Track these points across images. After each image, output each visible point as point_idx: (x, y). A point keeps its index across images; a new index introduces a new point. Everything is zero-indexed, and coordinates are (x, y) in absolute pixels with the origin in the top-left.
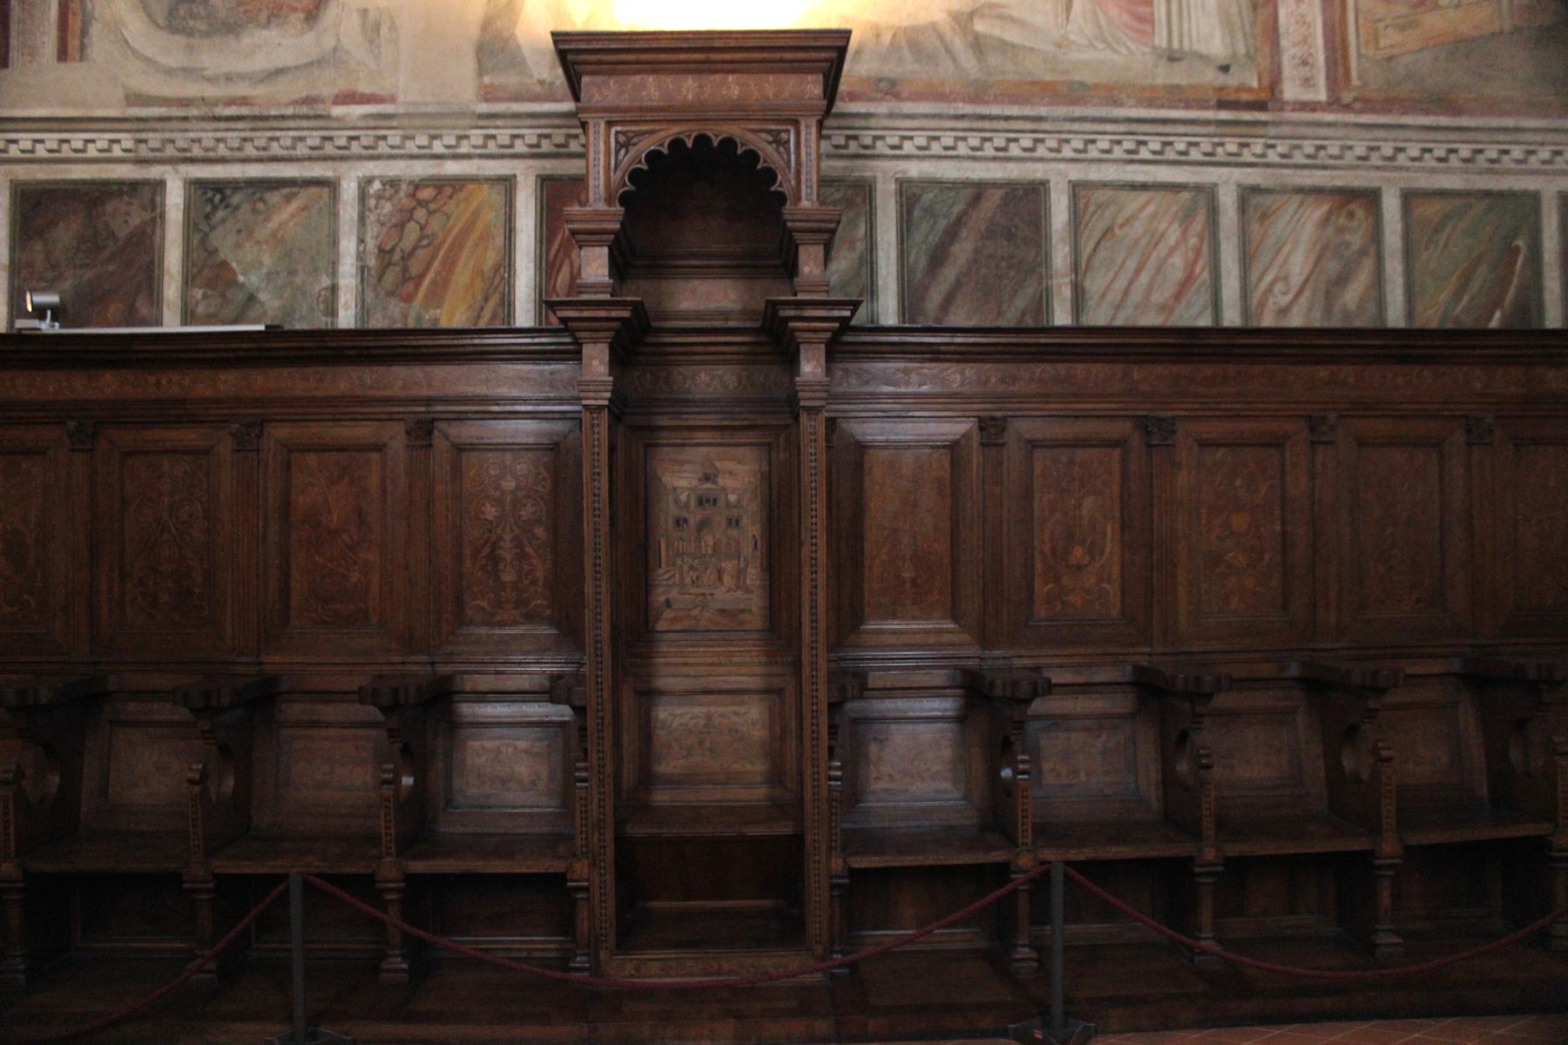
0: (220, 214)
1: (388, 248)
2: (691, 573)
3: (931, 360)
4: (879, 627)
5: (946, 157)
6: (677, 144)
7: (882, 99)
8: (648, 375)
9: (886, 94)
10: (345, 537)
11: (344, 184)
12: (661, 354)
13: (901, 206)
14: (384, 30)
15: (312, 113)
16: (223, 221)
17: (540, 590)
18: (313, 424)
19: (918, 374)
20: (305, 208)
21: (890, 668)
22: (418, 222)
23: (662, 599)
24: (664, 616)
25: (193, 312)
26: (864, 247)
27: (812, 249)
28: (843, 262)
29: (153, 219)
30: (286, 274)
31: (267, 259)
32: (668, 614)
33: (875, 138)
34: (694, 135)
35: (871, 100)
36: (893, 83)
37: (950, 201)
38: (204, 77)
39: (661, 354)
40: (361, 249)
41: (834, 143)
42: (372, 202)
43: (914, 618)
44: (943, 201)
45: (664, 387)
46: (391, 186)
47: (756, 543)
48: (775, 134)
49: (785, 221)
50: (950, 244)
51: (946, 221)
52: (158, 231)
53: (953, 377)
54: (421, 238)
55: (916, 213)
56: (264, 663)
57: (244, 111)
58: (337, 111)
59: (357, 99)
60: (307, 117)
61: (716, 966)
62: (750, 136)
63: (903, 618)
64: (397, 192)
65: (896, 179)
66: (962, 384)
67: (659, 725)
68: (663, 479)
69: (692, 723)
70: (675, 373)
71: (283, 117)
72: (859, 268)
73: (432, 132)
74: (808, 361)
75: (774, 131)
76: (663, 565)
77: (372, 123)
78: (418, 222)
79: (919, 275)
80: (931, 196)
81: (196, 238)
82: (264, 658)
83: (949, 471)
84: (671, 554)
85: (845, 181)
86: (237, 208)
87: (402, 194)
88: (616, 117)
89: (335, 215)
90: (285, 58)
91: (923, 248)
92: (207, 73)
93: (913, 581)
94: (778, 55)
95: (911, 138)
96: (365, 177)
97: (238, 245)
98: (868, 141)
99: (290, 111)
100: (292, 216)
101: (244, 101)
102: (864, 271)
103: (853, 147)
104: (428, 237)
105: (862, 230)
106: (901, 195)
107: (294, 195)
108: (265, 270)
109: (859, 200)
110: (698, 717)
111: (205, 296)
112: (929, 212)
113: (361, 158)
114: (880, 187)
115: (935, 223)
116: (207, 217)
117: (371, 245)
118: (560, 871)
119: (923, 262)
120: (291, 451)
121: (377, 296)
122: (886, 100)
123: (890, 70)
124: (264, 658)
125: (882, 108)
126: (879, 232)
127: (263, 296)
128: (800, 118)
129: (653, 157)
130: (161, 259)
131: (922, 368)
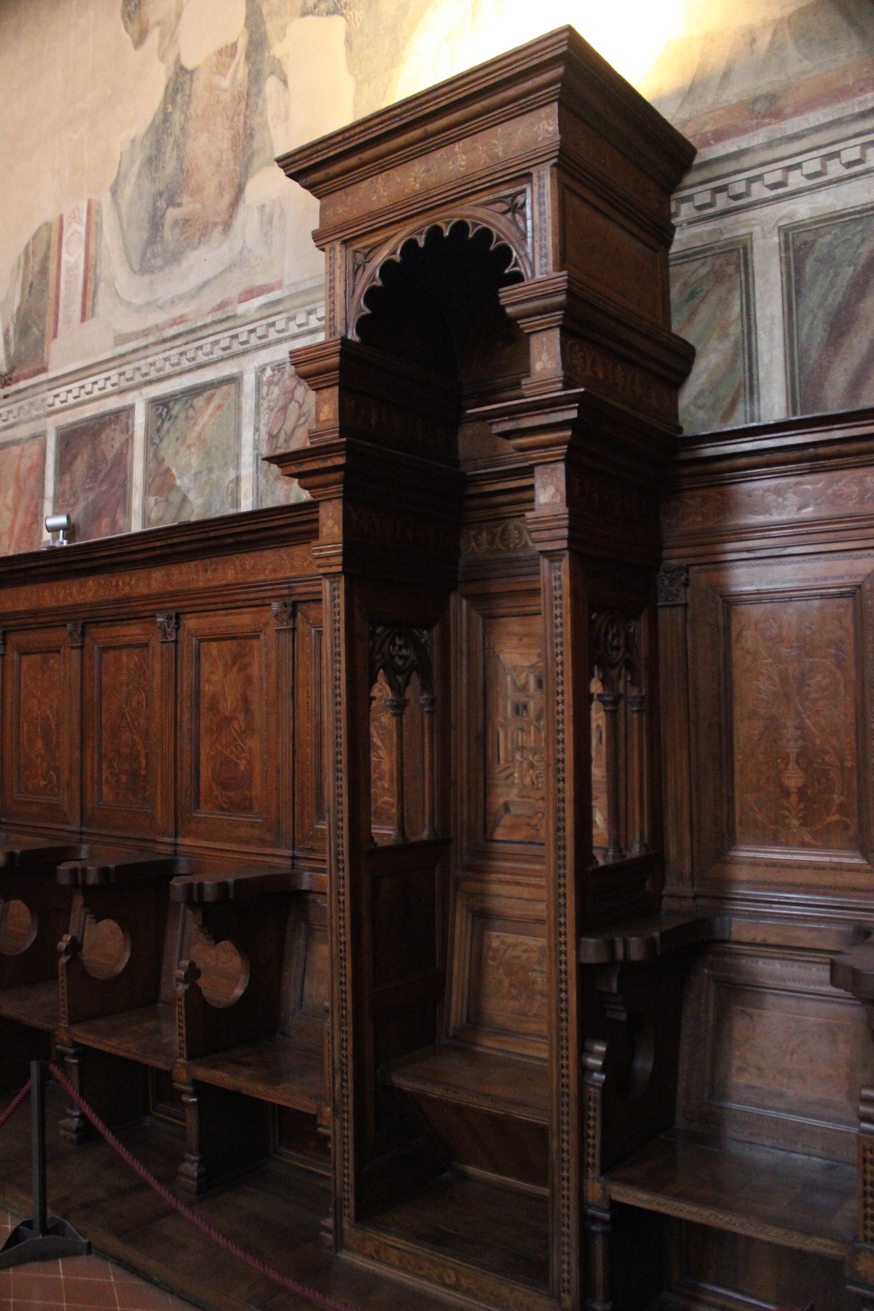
0: (167, 425)
1: (275, 433)
2: (531, 771)
3: (813, 471)
4: (752, 854)
5: (850, 177)
6: (410, 246)
7: (759, 126)
8: (485, 534)
9: (764, 117)
10: (236, 726)
11: (245, 377)
12: (489, 507)
13: (788, 264)
14: (276, 219)
15: (224, 316)
16: (168, 431)
17: (386, 785)
18: (211, 613)
19: (795, 493)
20: (219, 407)
21: (764, 916)
22: (297, 402)
23: (501, 800)
24: (503, 822)
25: (149, 519)
26: (739, 329)
27: (543, 337)
28: (712, 356)
29: (127, 440)
30: (206, 472)
31: (194, 461)
32: (506, 820)
33: (750, 181)
34: (426, 228)
35: (745, 131)
36: (772, 97)
37: (857, 239)
38: (158, 306)
39: (489, 507)
40: (257, 438)
41: (697, 203)
42: (265, 390)
43: (803, 845)
44: (845, 241)
45: (500, 546)
46: (279, 370)
47: (601, 734)
48: (510, 199)
49: (503, 307)
50: (859, 300)
51: (852, 268)
52: (130, 451)
53: (846, 490)
54: (299, 418)
55: (809, 268)
56: (180, 845)
57: (180, 328)
58: (241, 309)
59: (255, 293)
60: (221, 321)
61: (454, 1278)
62: (481, 213)
63: (787, 844)
64: (283, 374)
65: (780, 228)
66: (861, 499)
67: (491, 954)
68: (501, 657)
69: (525, 956)
70: (511, 527)
71: (205, 326)
72: (734, 361)
73: (309, 308)
74: (544, 487)
75: (506, 197)
76: (502, 762)
77: (265, 313)
78: (297, 402)
79: (814, 354)
80: (828, 238)
81: (153, 449)
82: (179, 841)
83: (851, 631)
84: (509, 746)
85: (711, 249)
86: (176, 417)
87: (286, 376)
88: (349, 233)
89: (238, 408)
90: (208, 272)
91: (820, 313)
92: (160, 303)
93: (801, 792)
94: (496, 98)
95: (799, 166)
96: (260, 367)
97: (177, 453)
98: (740, 188)
99: (209, 320)
100: (211, 416)
101: (181, 320)
102: (739, 365)
103: (722, 202)
104: (304, 414)
105: (736, 308)
106: (787, 249)
107: (212, 396)
108: (193, 472)
109: (731, 269)
110: (533, 951)
111: (156, 503)
112: (828, 261)
113: (257, 348)
114: (758, 245)
115: (837, 275)
116: (158, 430)
117: (264, 430)
118: (312, 1112)
119: (821, 332)
120: (200, 641)
121: (268, 481)
122: (763, 125)
123: (768, 83)
124: (179, 841)
125: (759, 137)
126: (758, 305)
127: (191, 496)
128: (531, 170)
129: (387, 267)
130: (131, 474)
131: (800, 483)
